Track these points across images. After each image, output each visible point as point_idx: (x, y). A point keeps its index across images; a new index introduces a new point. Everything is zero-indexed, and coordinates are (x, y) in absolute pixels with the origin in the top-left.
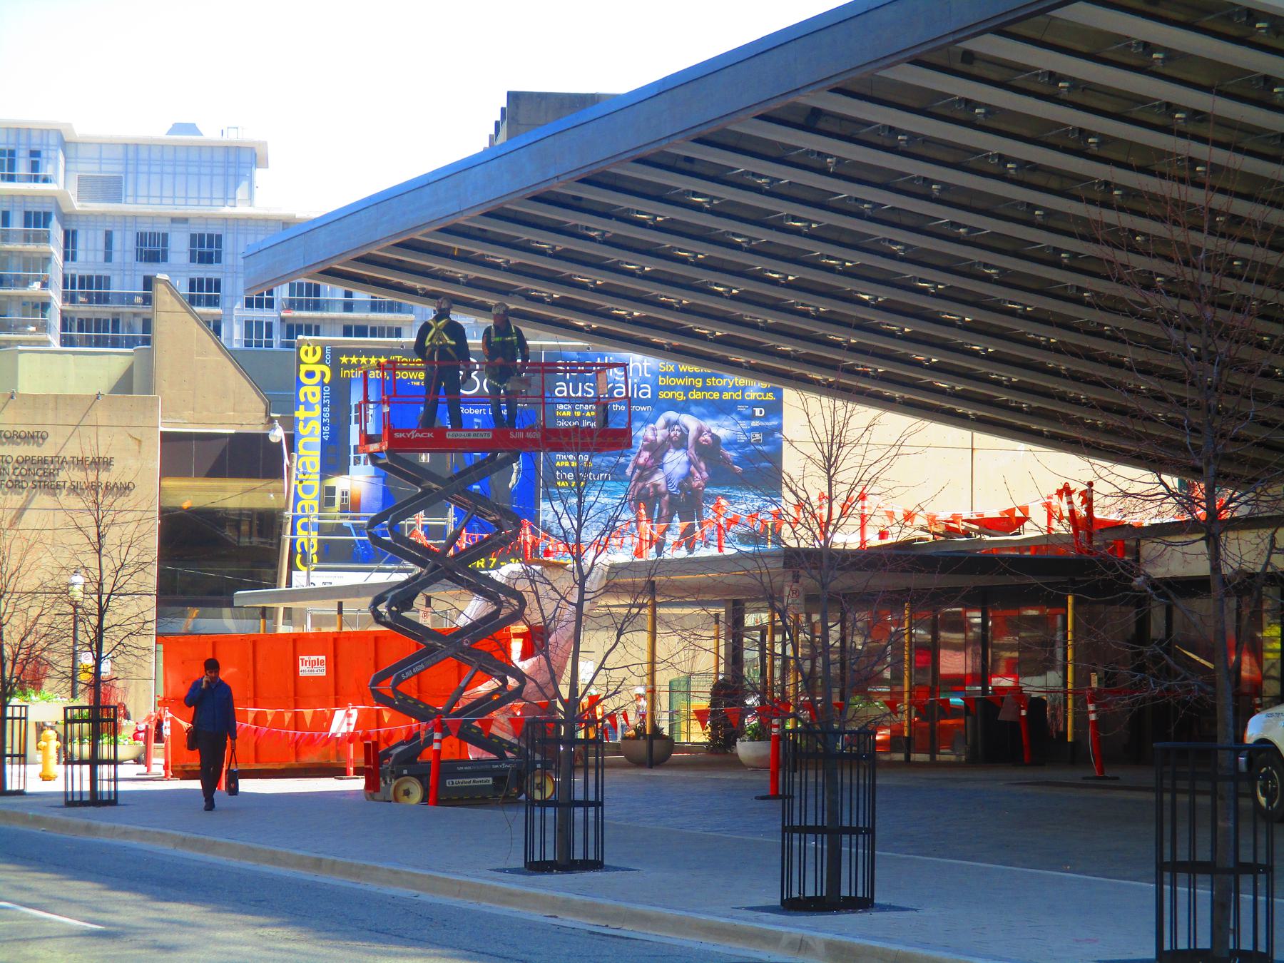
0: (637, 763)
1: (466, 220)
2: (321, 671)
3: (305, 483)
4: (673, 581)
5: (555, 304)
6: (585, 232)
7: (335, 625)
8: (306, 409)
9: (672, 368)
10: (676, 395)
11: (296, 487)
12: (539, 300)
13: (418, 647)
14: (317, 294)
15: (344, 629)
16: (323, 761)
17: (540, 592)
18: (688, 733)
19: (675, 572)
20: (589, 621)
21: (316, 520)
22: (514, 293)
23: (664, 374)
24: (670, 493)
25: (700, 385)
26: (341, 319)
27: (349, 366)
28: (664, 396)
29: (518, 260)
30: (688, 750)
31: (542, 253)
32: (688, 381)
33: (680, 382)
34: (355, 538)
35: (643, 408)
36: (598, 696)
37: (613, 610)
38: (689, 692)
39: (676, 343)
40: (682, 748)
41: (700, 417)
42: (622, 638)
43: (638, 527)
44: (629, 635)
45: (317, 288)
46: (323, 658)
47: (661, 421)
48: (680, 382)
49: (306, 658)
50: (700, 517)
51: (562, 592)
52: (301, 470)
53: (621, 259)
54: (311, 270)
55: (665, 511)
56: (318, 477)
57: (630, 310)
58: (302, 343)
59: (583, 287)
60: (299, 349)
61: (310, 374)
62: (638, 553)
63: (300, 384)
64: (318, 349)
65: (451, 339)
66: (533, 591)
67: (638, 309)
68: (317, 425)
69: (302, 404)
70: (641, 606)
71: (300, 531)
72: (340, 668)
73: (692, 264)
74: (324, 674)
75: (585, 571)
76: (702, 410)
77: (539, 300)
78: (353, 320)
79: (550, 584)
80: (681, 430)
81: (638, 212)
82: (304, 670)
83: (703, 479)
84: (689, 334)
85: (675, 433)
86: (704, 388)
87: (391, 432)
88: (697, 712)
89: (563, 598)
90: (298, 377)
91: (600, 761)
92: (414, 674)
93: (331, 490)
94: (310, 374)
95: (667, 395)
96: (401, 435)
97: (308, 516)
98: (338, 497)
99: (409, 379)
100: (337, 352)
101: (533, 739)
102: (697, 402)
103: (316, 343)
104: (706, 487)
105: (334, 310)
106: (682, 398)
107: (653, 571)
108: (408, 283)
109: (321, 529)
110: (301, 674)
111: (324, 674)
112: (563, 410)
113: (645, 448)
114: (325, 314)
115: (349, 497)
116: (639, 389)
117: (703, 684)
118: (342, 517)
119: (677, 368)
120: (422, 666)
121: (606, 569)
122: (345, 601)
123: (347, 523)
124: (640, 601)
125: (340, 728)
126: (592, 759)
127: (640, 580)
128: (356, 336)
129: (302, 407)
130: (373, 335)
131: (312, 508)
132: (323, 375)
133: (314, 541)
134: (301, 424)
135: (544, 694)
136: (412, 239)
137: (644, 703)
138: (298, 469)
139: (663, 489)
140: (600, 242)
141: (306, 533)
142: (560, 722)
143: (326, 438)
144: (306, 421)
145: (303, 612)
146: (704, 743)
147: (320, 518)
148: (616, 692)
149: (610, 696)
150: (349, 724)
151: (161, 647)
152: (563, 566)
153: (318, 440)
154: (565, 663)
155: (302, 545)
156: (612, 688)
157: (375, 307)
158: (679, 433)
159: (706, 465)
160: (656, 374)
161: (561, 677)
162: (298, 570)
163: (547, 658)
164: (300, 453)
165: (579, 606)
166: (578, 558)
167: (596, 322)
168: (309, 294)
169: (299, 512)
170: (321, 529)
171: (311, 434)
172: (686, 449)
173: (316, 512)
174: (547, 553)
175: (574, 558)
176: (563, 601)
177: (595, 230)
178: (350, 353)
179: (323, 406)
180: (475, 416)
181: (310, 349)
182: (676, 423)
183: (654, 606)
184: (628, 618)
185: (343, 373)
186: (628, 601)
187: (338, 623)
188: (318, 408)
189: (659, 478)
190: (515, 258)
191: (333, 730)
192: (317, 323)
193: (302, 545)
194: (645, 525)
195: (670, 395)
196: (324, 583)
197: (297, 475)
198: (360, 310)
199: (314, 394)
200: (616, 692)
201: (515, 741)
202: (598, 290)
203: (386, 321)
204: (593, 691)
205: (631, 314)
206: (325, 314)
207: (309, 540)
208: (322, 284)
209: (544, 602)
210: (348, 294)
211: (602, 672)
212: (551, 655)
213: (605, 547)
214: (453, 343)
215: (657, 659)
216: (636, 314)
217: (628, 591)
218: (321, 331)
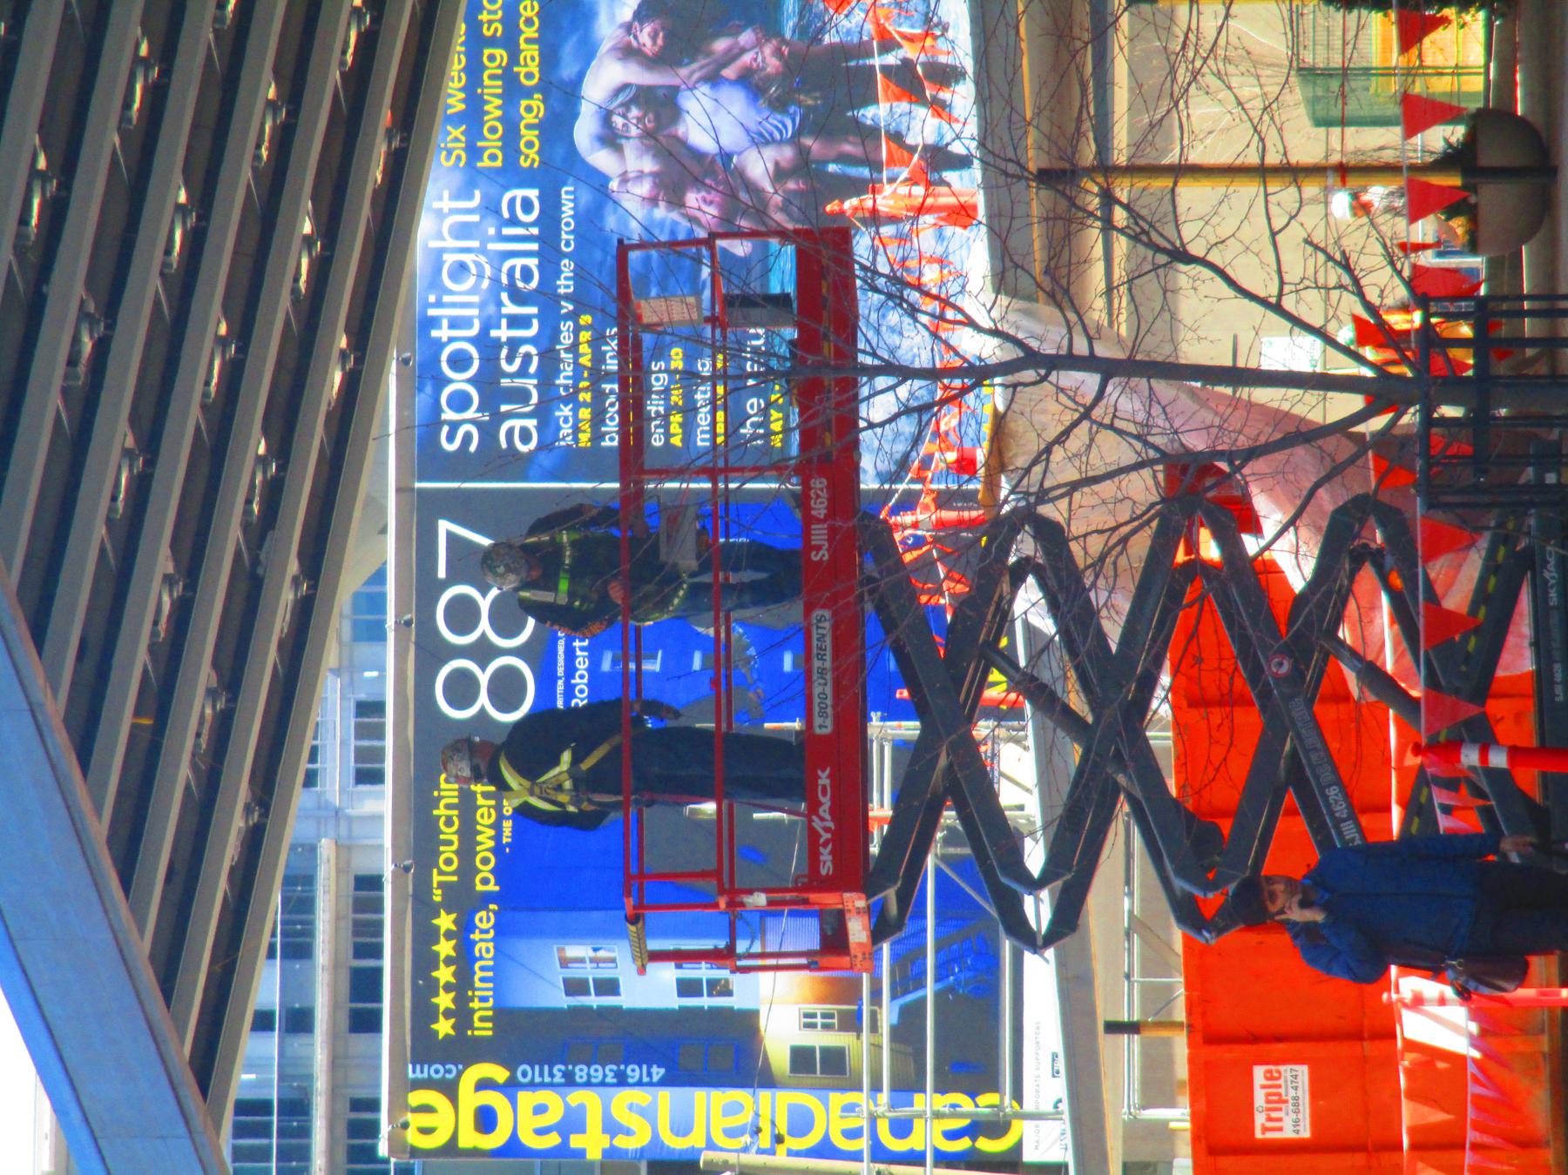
0: (1541, 211)
1: (55, 690)
2: (1296, 1079)
3: (782, 1128)
4: (1038, 112)
5: (282, 449)
6: (82, 369)
7: (1167, 1043)
8: (582, 1130)
9: (457, 132)
10: (529, 118)
11: (791, 1153)
12: (274, 492)
13: (1292, 812)
14: (263, 1107)
15: (1180, 1015)
16: (1546, 1072)
17: (1074, 475)
18: (1458, 71)
19: (1012, 104)
20: (1149, 342)
21: (884, 1097)
22: (255, 562)
23: (474, 152)
24: (798, 133)
25: (500, 53)
26: (334, 1038)
27: (462, 1015)
28: (533, 153)
29: (165, 551)
30: (1507, 73)
31: (141, 488)
32: (492, 88)
33: (493, 108)
34: (930, 990)
35: (568, 209)
36: (1357, 320)
37: (1119, 273)
38: (1345, 73)
39: (386, 117)
40: (1505, 85)
41: (588, 52)
42: (1196, 249)
43: (893, 219)
44: (1188, 231)
45: (243, 1108)
46: (1259, 1073)
47: (602, 160)
48: (493, 108)
49: (1260, 1119)
50: (863, 50)
51: (1069, 417)
52: (747, 1139)
53: (156, 268)
54: (198, 1120)
55: (848, 148)
56: (765, 1095)
57: (296, 243)
58: (397, 1144)
59: (234, 374)
60: (415, 1152)
61: (486, 1121)
62: (961, 214)
63: (513, 1147)
64: (417, 1098)
65: (557, 762)
66: (1069, 494)
67: (294, 223)
68: (624, 1101)
69: (565, 1140)
70: (1108, 199)
71: (914, 1142)
72: (1018, 779)
73: (166, 72)
74: (1303, 1071)
75: (1012, 353)
76: (568, 50)
77: (274, 492)
78: (335, 1007)
79: (1048, 450)
80: (627, 105)
81: (24, 220)
82: (1295, 1124)
83: (758, 44)
84: (360, 78)
85: (630, 123)
86: (510, 41)
87: (814, 882)
88: (1405, 46)
89: (1086, 415)
90: (497, 1153)
91: (1537, 305)
92: (1353, 816)
93: (802, 1059)
94: (486, 1121)
95: (530, 145)
96: (826, 855)
97: (873, 1120)
98: (820, 1039)
99: (498, 850)
100: (424, 1048)
101: (1476, 489)
102: (549, 60)
103: (399, 1104)
104: (779, 34)
105: (309, 1060)
106: (537, 102)
107: (1012, 168)
108: (230, 852)
109: (907, 1085)
110: (1306, 1133)
111: (1303, 1071)
112: (576, 430)
113: (677, 202)
114: (321, 1085)
115: (819, 1008)
116: (513, 221)
117: (1322, 37)
118: (874, 1028)
119: (458, 119)
120: (1333, 792)
121: (1004, 300)
122: (1104, 1014)
123: (888, 1015)
124: (1094, 203)
125: (1455, 1028)
126: (1529, 327)
127: (1037, 201)
128: (378, 998)
129: (576, 1142)
130: (377, 952)
131: (849, 1109)
132: (484, 1085)
133: (942, 1102)
134: (622, 1142)
135: (1352, 460)
136: (110, 841)
137: (1377, 193)
138: (745, 1150)
139: (788, 153)
140: (111, 327)
141: (918, 1125)
142: (1428, 421)
143: (658, 1072)
144: (612, 1127)
145: (1137, 1131)
146: (1489, 26)
147: (876, 1088)
148: (1346, 265)
149: (1356, 281)
150: (1442, 1001)
151: (987, 382)
152: (999, 420)
153: (665, 1096)
154: (1263, 408)
155: (952, 1135)
156: (1334, 275)
157: (297, 948)
158: (635, 112)
159: (717, 35)
160: (472, 176)
161: (1302, 420)
162: (1018, 1148)
163: (1251, 454)
164: (701, 1144)
165: (1108, 369)
166: (979, 373)
167: (332, 338)
168: (264, 1131)
169: (863, 1144)
170: (907, 1085)
171: (648, 1114)
172: (674, 91)
173: (861, 1098)
174: (965, 465)
175: (978, 384)
176: (1097, 413)
177: (76, 341)
178: (424, 1013)
179: (570, 1082)
180: (594, 669)
181: (417, 1121)
182: (606, 117)
183: (1105, 168)
184: (1140, 234)
185: (482, 1029)
186: (1094, 234)
187: (1165, 1034)
188: (577, 1097)
189: (758, 166)
190: (159, 560)
191: (1459, 1044)
192: (344, 1106)
193: (952, 1135)
194: (890, 198)
195: (529, 135)
196: (1055, 1074)
197: (761, 1152)
198: (307, 989)
199: (540, 1110)
200: (1346, 265)
201: (1484, 543)
202: (244, 330)
203: (338, 918)
204: (1346, 334)
205: (308, 241)
206: (321, 1085)
207: (938, 1115)
208: (234, 1094)
209: (1098, 466)
210: (263, 1022)
211: (1288, 303)
212: (1243, 442)
213: (946, 303)
214: (566, 757)
215: (1253, 158)
216: (307, 228)
217: (1068, 236)
218: (362, 1094)
